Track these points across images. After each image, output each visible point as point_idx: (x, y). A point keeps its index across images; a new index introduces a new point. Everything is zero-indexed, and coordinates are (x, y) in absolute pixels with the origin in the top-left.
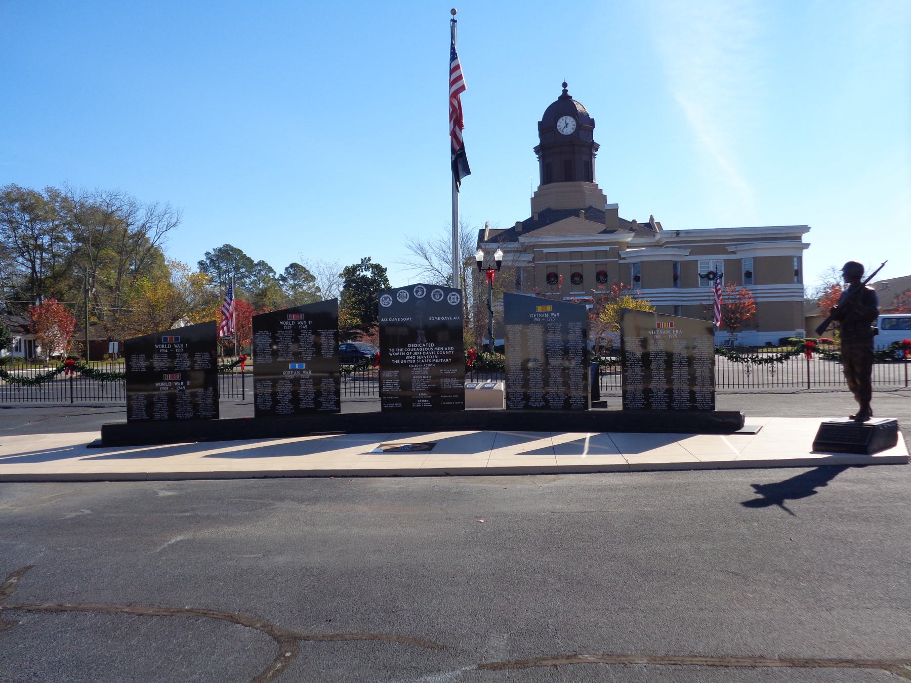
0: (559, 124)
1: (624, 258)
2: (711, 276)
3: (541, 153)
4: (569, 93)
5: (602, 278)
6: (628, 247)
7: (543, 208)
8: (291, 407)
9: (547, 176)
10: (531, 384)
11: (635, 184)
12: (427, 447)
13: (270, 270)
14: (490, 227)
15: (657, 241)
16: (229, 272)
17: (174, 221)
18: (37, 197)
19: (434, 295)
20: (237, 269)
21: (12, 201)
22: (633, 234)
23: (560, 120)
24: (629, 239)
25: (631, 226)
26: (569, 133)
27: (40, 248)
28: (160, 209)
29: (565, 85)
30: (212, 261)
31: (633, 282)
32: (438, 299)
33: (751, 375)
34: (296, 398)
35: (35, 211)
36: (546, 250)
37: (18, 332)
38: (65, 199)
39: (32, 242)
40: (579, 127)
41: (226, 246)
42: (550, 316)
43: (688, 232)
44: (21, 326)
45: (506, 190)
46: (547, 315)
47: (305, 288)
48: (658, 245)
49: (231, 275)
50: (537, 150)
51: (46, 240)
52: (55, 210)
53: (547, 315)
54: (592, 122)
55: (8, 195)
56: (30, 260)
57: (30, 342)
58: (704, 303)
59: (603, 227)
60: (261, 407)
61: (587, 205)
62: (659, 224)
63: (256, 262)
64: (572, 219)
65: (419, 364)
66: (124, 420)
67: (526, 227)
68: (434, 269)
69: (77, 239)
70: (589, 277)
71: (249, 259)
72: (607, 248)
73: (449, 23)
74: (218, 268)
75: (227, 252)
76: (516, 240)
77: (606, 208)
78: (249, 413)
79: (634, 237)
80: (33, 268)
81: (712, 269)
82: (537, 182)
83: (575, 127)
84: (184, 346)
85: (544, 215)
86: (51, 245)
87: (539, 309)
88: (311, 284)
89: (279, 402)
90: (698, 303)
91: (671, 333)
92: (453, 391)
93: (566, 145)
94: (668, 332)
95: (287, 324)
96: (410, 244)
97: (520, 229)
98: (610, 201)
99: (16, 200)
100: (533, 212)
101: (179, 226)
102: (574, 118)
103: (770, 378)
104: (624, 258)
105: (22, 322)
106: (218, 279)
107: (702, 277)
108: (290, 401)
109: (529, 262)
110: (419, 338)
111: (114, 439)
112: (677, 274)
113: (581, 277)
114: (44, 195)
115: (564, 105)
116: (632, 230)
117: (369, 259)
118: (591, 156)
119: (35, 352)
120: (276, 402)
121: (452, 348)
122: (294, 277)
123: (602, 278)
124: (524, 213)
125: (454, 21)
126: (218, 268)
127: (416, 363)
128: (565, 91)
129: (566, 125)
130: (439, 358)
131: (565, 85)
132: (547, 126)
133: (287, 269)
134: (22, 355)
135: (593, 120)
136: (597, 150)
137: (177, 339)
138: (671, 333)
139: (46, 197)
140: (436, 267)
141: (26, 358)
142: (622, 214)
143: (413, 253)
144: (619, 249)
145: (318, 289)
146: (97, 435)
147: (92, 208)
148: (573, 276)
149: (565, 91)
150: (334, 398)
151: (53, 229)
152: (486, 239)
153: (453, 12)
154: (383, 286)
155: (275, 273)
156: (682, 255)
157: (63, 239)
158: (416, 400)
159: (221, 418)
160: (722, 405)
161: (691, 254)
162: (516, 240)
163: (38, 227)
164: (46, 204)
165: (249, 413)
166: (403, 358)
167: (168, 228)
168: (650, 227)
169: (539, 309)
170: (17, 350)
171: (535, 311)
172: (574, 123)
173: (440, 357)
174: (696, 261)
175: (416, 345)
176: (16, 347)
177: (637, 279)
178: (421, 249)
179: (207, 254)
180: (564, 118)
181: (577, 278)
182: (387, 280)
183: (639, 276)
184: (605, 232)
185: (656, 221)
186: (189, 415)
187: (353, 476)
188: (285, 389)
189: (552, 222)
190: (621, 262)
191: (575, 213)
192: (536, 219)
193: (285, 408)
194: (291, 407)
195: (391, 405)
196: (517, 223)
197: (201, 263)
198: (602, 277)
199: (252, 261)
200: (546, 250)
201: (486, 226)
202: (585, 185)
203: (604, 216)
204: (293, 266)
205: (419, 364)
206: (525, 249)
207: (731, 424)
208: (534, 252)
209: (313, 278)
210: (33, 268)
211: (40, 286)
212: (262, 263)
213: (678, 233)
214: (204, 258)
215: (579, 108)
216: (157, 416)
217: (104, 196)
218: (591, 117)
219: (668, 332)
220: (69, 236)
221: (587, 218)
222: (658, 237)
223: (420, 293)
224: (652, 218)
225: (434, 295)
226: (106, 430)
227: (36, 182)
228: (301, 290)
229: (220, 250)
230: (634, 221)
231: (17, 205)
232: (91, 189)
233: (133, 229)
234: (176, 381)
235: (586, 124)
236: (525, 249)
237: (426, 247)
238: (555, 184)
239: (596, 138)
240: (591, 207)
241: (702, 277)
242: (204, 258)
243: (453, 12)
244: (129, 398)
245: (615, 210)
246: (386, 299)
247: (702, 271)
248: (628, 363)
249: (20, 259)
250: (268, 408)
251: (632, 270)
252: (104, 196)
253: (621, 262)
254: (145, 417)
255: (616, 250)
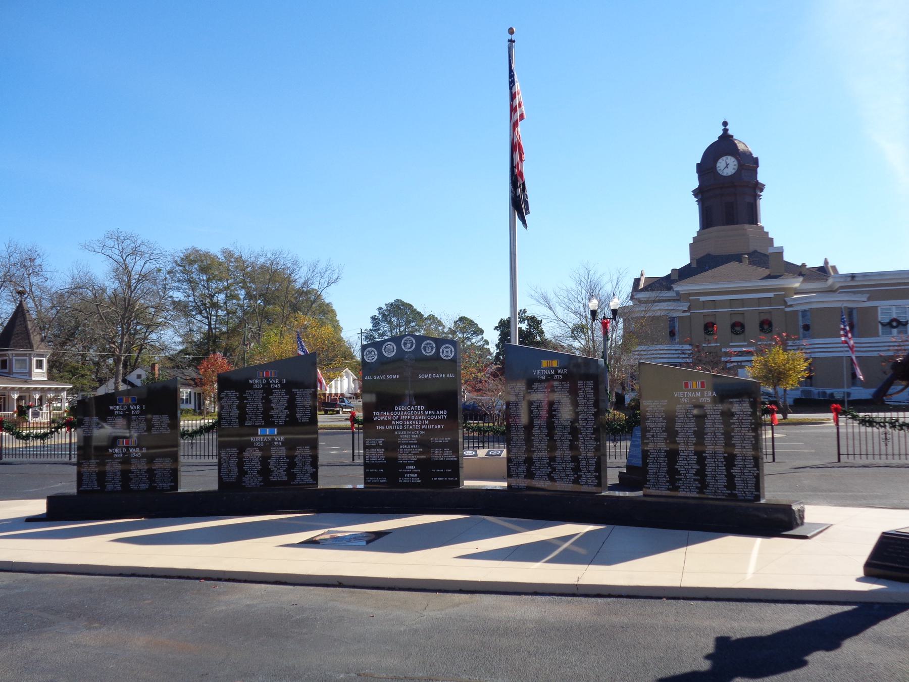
0: (718, 164)
1: (791, 306)
2: (894, 324)
3: (700, 196)
4: (730, 132)
5: (766, 327)
6: (796, 294)
7: (702, 254)
8: (261, 479)
9: (707, 220)
10: (708, 438)
11: (803, 226)
12: (373, 536)
13: (440, 323)
14: (645, 276)
15: (830, 286)
16: (400, 327)
17: (335, 277)
18: (213, 258)
19: (425, 348)
20: (408, 323)
21: (192, 263)
22: (801, 279)
23: (720, 161)
24: (797, 285)
25: (800, 271)
26: (730, 174)
27: (216, 306)
28: (321, 266)
29: (725, 124)
30: (384, 315)
31: (802, 330)
32: (429, 352)
33: (890, 444)
34: (265, 471)
35: (211, 272)
36: (702, 299)
37: (188, 385)
38: (239, 260)
39: (208, 300)
40: (741, 167)
41: (398, 301)
42: (556, 373)
43: (865, 275)
44: (193, 380)
45: (667, 238)
46: (553, 372)
47: (474, 341)
48: (831, 291)
49: (402, 329)
50: (696, 193)
51: (221, 297)
52: (228, 270)
53: (553, 372)
54: (756, 161)
55: (187, 257)
56: (207, 318)
57: (199, 394)
58: (882, 354)
59: (767, 272)
60: (226, 478)
61: (751, 249)
62: (834, 268)
63: (425, 316)
64: (734, 264)
65: (407, 430)
66: (73, 490)
67: (683, 274)
68: (558, 319)
69: (249, 296)
70: (752, 326)
71: (419, 313)
72: (771, 295)
73: (507, 44)
74: (390, 322)
75: (398, 306)
76: (670, 289)
77: (771, 250)
78: (212, 484)
79: (802, 282)
80: (210, 325)
81: (894, 316)
82: (697, 227)
83: (736, 167)
84: (141, 407)
85: (703, 261)
86: (225, 303)
87: (545, 364)
88: (480, 337)
89: (246, 473)
90: (875, 354)
91: (702, 395)
92: (445, 464)
93: (728, 188)
94: (698, 394)
95: (256, 382)
96: (533, 293)
97: (676, 277)
98: (776, 244)
99: (194, 262)
100: (691, 259)
101: (340, 281)
102: (737, 159)
103: (883, 447)
104: (791, 306)
105: (194, 375)
106: (389, 334)
107: (883, 325)
108: (258, 472)
109: (685, 311)
110: (407, 399)
111: (64, 512)
112: (855, 321)
113: (742, 326)
114: (220, 256)
115: (725, 144)
116: (801, 274)
117: (525, 311)
118: (756, 197)
119: (204, 403)
120: (242, 473)
121: (445, 412)
122: (463, 331)
123: (766, 327)
124: (683, 259)
125: (512, 41)
126: (390, 322)
127: (403, 430)
128: (726, 131)
129: (727, 166)
130: (429, 424)
131: (725, 124)
132: (706, 168)
133: (456, 322)
134: (191, 406)
135: (757, 159)
136: (762, 190)
137: (133, 400)
138: (702, 395)
139: (221, 257)
140: (561, 317)
141: (195, 410)
142: (787, 258)
143: (534, 302)
144: (784, 296)
145: (487, 342)
146: (39, 507)
147: (262, 267)
148: (734, 326)
149: (726, 131)
150: (311, 470)
151: (227, 288)
152: (641, 286)
153: (511, 31)
154: (539, 338)
155: (444, 327)
156: (860, 301)
157: (236, 297)
158: (402, 475)
159: (179, 491)
160: (773, 492)
161: (869, 299)
162: (670, 289)
163: (214, 286)
164: (221, 264)
165: (212, 484)
166: (389, 422)
167: (329, 284)
168: (823, 271)
169: (545, 364)
170: (187, 402)
171: (539, 367)
172: (736, 163)
173: (431, 422)
174: (876, 308)
175: (403, 408)
176: (187, 399)
177: (806, 328)
178: (546, 299)
179: (380, 309)
180: (724, 158)
181: (738, 328)
182: (543, 332)
183: (807, 324)
184: (769, 277)
185: (831, 264)
186: (144, 486)
187: (219, 580)
188: (253, 455)
189: (711, 268)
190: (788, 309)
191: (738, 258)
192: (694, 265)
193: (253, 480)
194: (261, 479)
195: (374, 480)
196: (673, 270)
197: (373, 318)
198: (766, 326)
199: (422, 316)
200: (702, 299)
201: (642, 275)
202: (749, 228)
203: (768, 259)
204: (462, 319)
205: (407, 430)
206: (679, 298)
207: (780, 523)
208: (690, 301)
209: (482, 332)
210: (210, 325)
211: (214, 342)
212: (432, 318)
213: (853, 276)
214: (376, 313)
215: (741, 147)
216: (109, 487)
217: (269, 255)
218: (755, 156)
219: (698, 394)
220: (242, 293)
221: (750, 263)
222: (830, 281)
223: (409, 345)
224: (826, 262)
225: (425, 348)
226: (53, 502)
227: (214, 246)
228: (469, 343)
229: (392, 304)
230: (804, 265)
231: (196, 266)
232: (257, 250)
233: (298, 285)
234: (132, 447)
235: (749, 164)
236: (679, 298)
237: (551, 296)
238: (715, 228)
239: (761, 177)
240: (755, 252)
241: (883, 325)
242: (376, 313)
243: (511, 31)
244: (219, 455)
245: (780, 253)
246: (370, 353)
247: (882, 317)
248: (649, 435)
249: (199, 317)
250: (233, 479)
251: (800, 318)
252: (269, 255)
253: (788, 309)
254: (96, 487)
255: (782, 297)
